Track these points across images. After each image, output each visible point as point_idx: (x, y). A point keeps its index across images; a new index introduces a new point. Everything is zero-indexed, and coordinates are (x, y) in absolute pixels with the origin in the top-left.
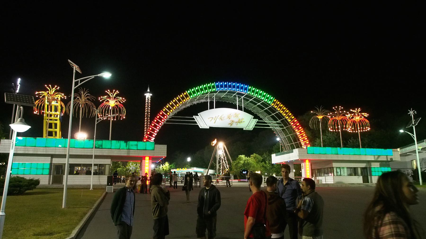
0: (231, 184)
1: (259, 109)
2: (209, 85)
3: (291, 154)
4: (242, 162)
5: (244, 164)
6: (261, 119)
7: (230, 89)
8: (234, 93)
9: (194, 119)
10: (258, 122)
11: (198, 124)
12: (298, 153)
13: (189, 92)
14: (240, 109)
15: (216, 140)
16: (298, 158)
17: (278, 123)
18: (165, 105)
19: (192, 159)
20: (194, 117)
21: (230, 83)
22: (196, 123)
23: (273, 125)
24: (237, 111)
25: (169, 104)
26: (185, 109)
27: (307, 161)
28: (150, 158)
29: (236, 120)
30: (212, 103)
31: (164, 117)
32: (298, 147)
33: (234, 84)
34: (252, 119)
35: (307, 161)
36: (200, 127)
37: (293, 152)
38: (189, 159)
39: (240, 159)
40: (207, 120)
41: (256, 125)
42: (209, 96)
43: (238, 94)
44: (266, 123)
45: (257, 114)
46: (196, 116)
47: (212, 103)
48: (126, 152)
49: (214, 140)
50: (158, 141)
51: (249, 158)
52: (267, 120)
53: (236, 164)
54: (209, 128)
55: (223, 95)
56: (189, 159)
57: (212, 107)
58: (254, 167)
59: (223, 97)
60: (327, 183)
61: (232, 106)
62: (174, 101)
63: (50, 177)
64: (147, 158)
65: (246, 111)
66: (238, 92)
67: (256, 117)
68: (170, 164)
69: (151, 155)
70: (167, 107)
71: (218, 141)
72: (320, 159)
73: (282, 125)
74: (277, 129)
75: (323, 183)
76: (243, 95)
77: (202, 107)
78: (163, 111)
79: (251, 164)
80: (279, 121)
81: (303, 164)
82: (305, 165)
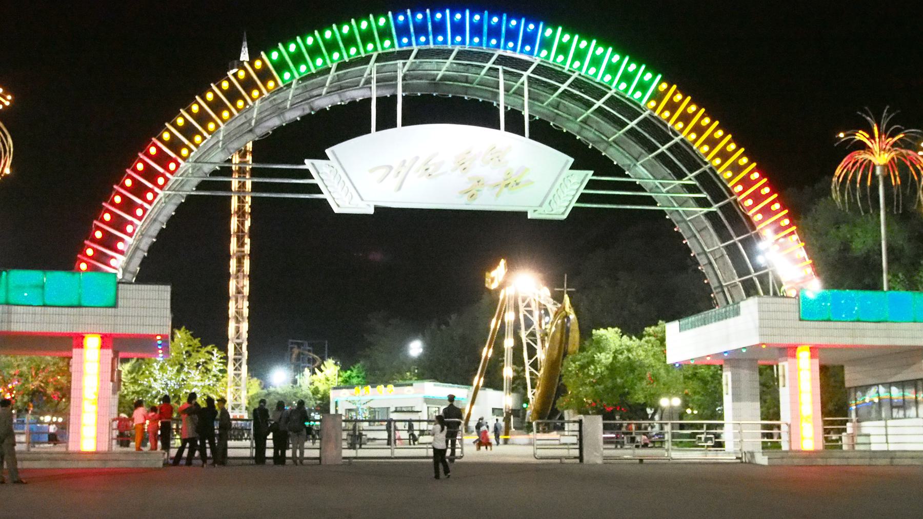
0: (458, 452)
1: (607, 127)
2: (364, 25)
3: (731, 321)
4: (605, 358)
5: (612, 369)
6: (620, 171)
7: (423, 39)
8: (486, 57)
9: (307, 174)
10: (591, 185)
11: (325, 195)
12: (756, 315)
13: (275, 55)
14: (514, 123)
15: (503, 262)
16: (755, 341)
17: (690, 189)
18: (171, 117)
19: (429, 347)
20: (308, 164)
21: (420, 16)
22: (316, 189)
23: (668, 194)
24: (500, 137)
25: (189, 111)
26: (279, 130)
27: (803, 354)
28: (107, 340)
29: (494, 174)
30: (387, 104)
31: (166, 168)
32: (750, 289)
33: (495, 20)
34: (568, 172)
35: (803, 354)
36: (336, 210)
37: (737, 313)
38: (416, 348)
39: (600, 346)
40: (361, 177)
41: (583, 198)
42: (374, 75)
43: (502, 60)
44: (640, 188)
45: (600, 147)
46: (318, 162)
47: (387, 104)
48: (14, 318)
49: (493, 265)
50: (148, 273)
51: (634, 342)
52: (641, 171)
53: (582, 367)
54: (371, 211)
55: (443, 68)
56: (416, 348)
57: (387, 122)
58: (655, 378)
59: (444, 78)
60: (892, 448)
61: (480, 113)
62: (210, 96)
63: (424, 458)
64: (92, 343)
65: (544, 132)
66: (501, 52)
67: (584, 156)
68: (344, 368)
69: (108, 330)
70: (180, 122)
71: (510, 266)
72: (859, 341)
73: (704, 195)
74: (688, 214)
75: (874, 448)
76: (525, 65)
77: (348, 122)
78: (160, 139)
79: (642, 365)
80: (690, 179)
81: (784, 367)
82: (795, 370)
